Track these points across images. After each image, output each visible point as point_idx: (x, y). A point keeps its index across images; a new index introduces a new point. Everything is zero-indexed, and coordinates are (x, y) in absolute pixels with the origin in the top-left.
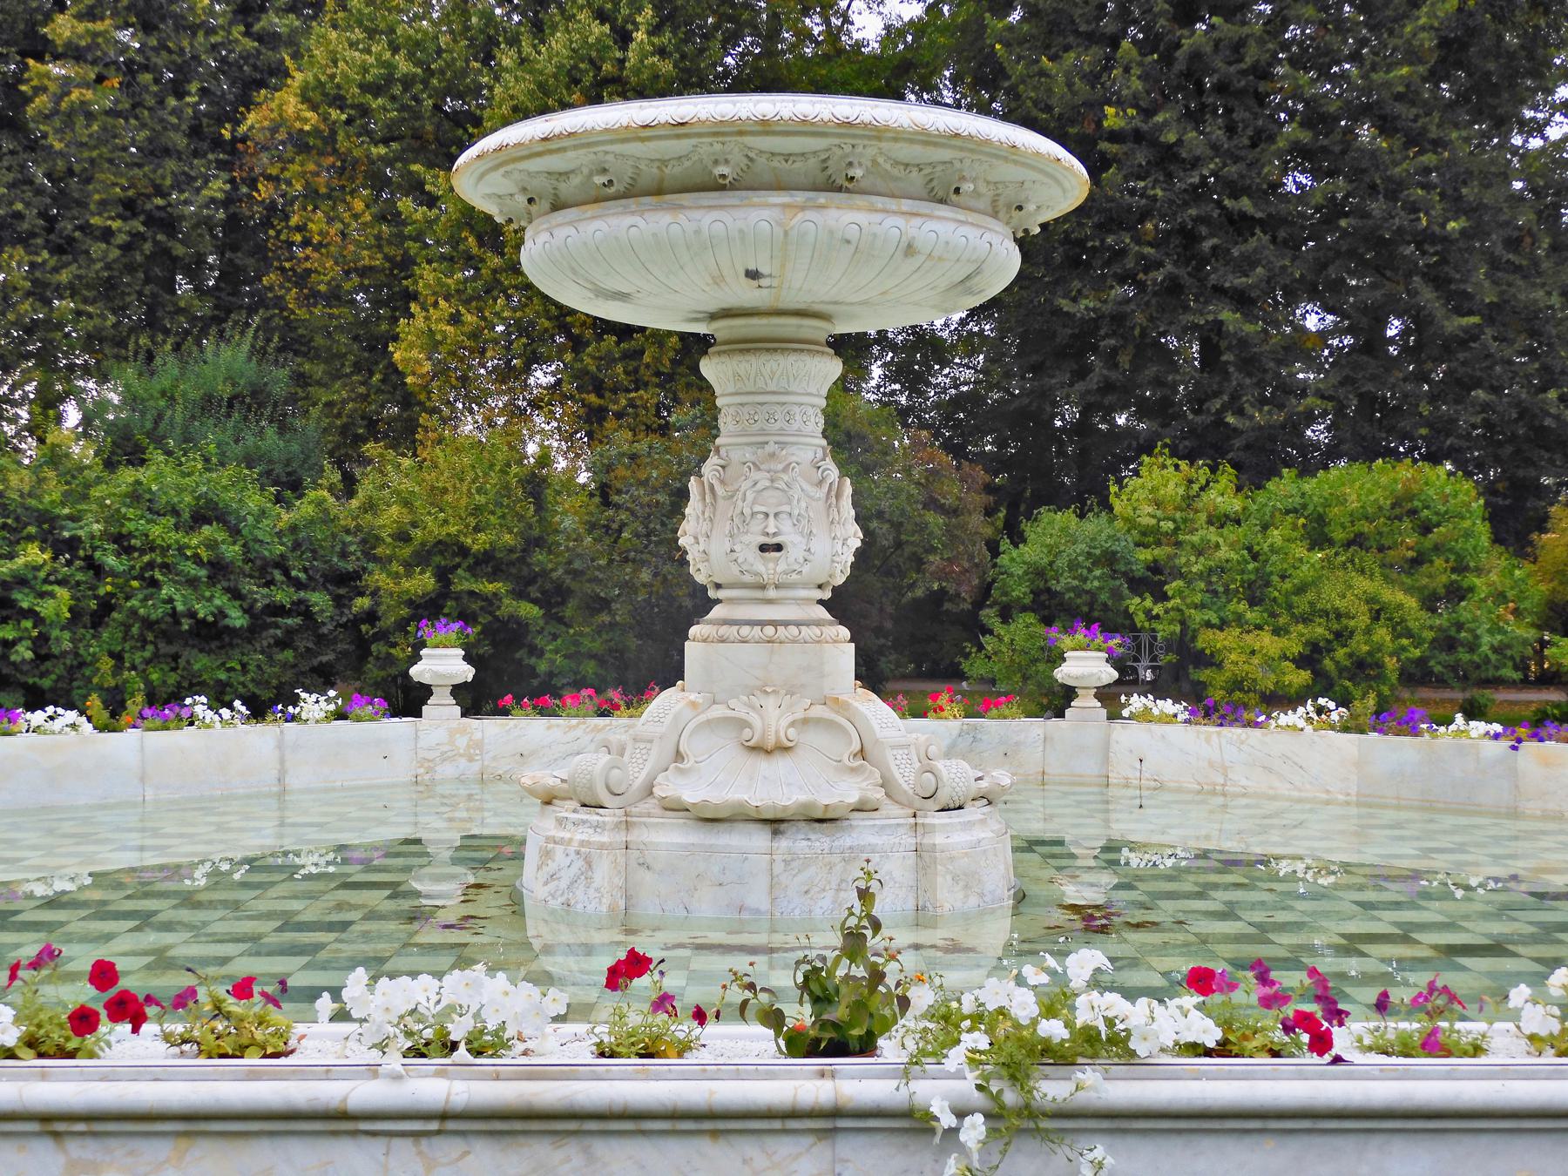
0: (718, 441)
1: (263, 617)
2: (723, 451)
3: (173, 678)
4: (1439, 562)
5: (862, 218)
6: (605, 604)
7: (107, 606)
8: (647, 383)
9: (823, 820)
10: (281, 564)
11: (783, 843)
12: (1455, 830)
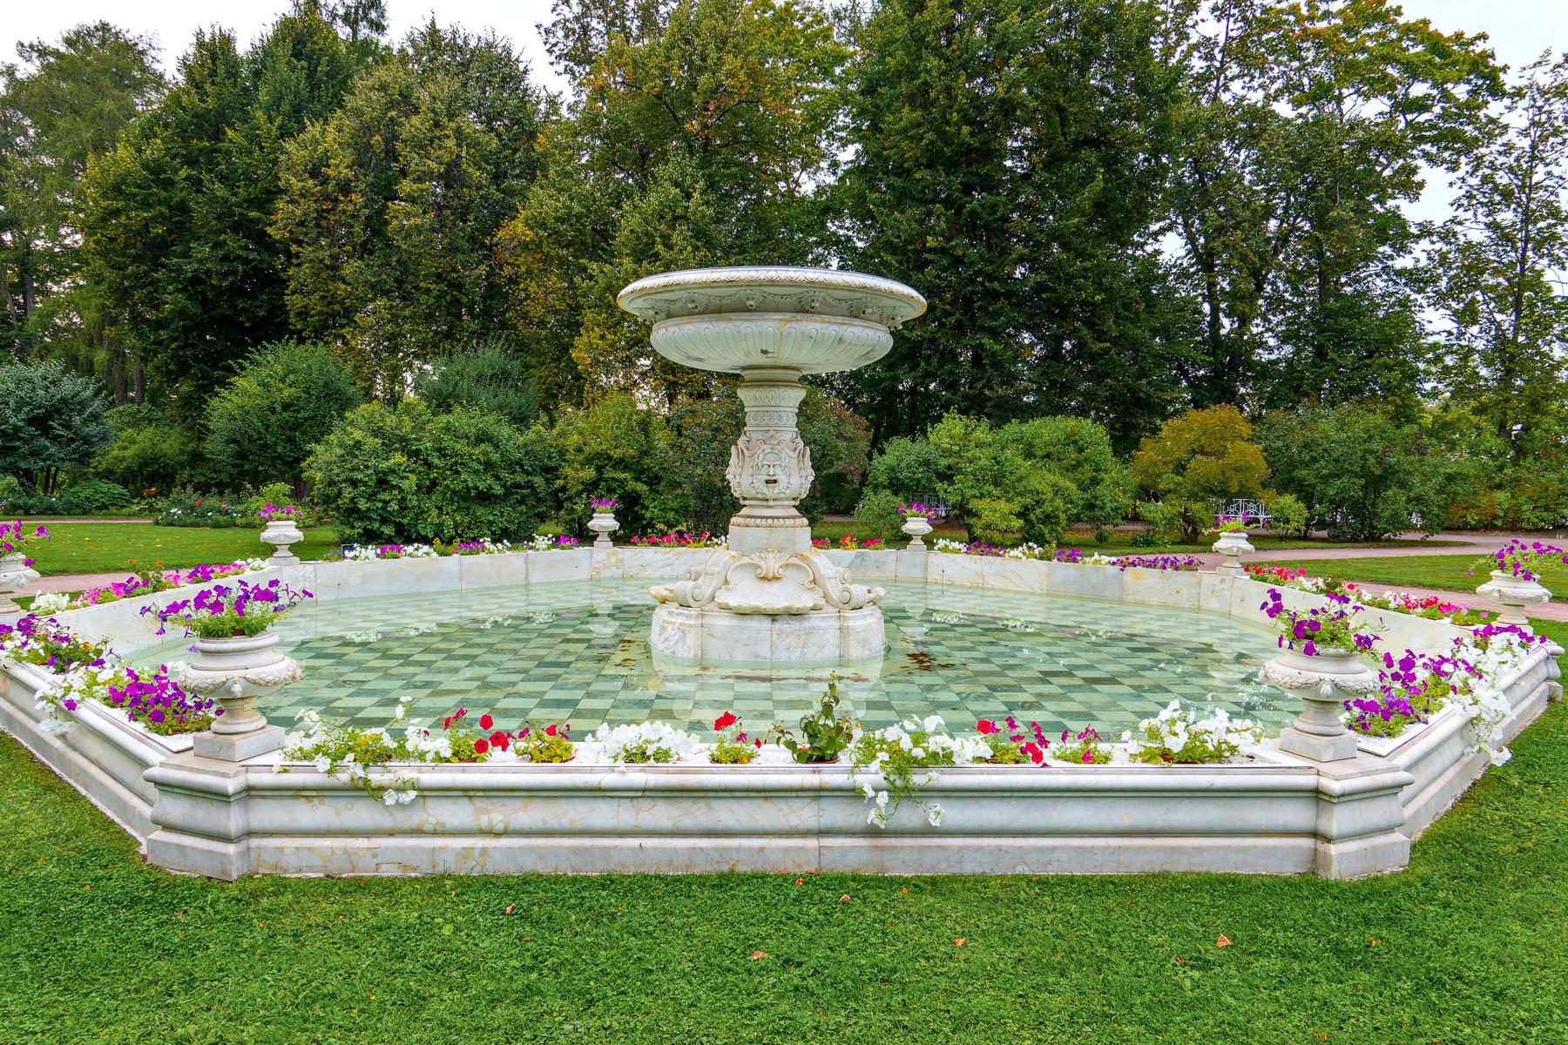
1: (510, 490)
3: (467, 519)
4: (1087, 467)
5: (818, 326)
6: (679, 485)
7: (434, 483)
8: (711, 404)
9: (796, 615)
10: (519, 463)
11: (777, 625)
12: (1096, 610)
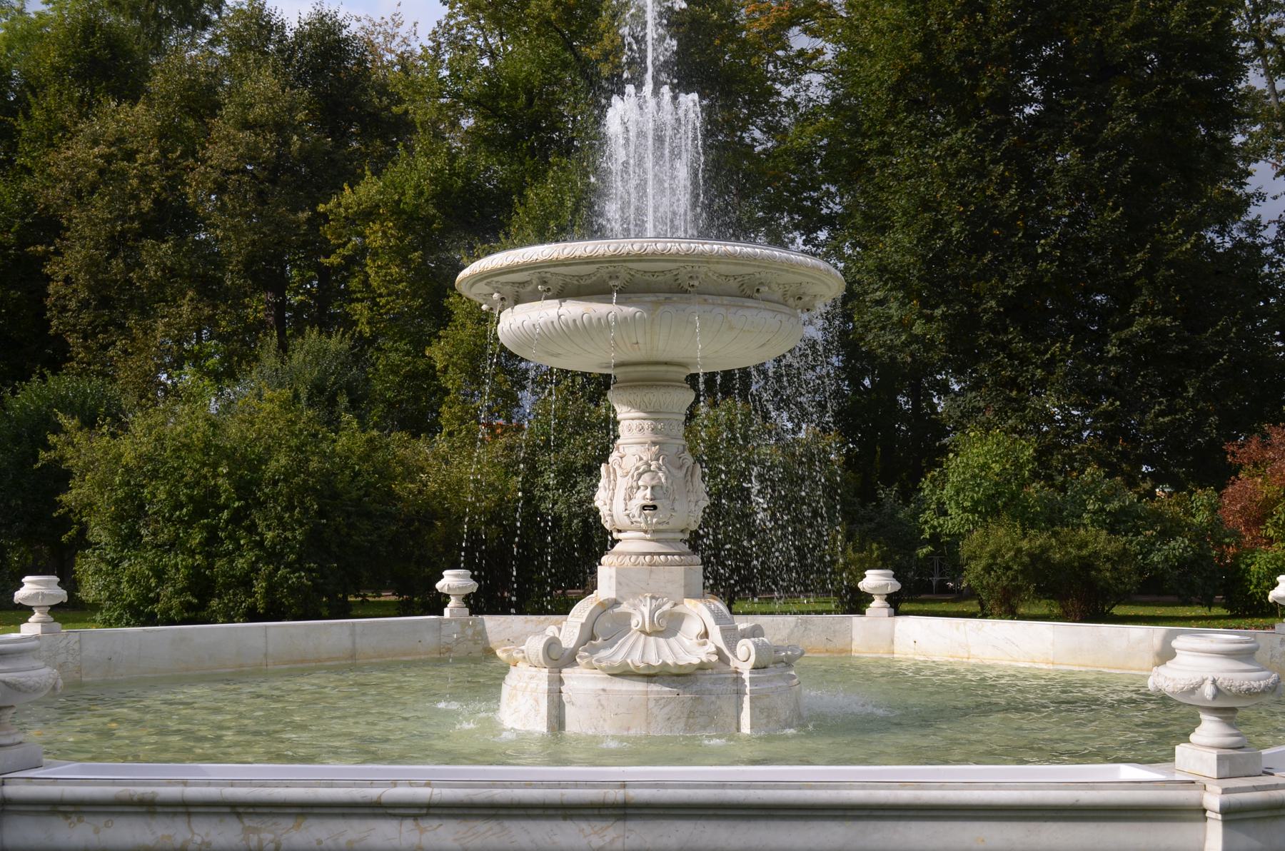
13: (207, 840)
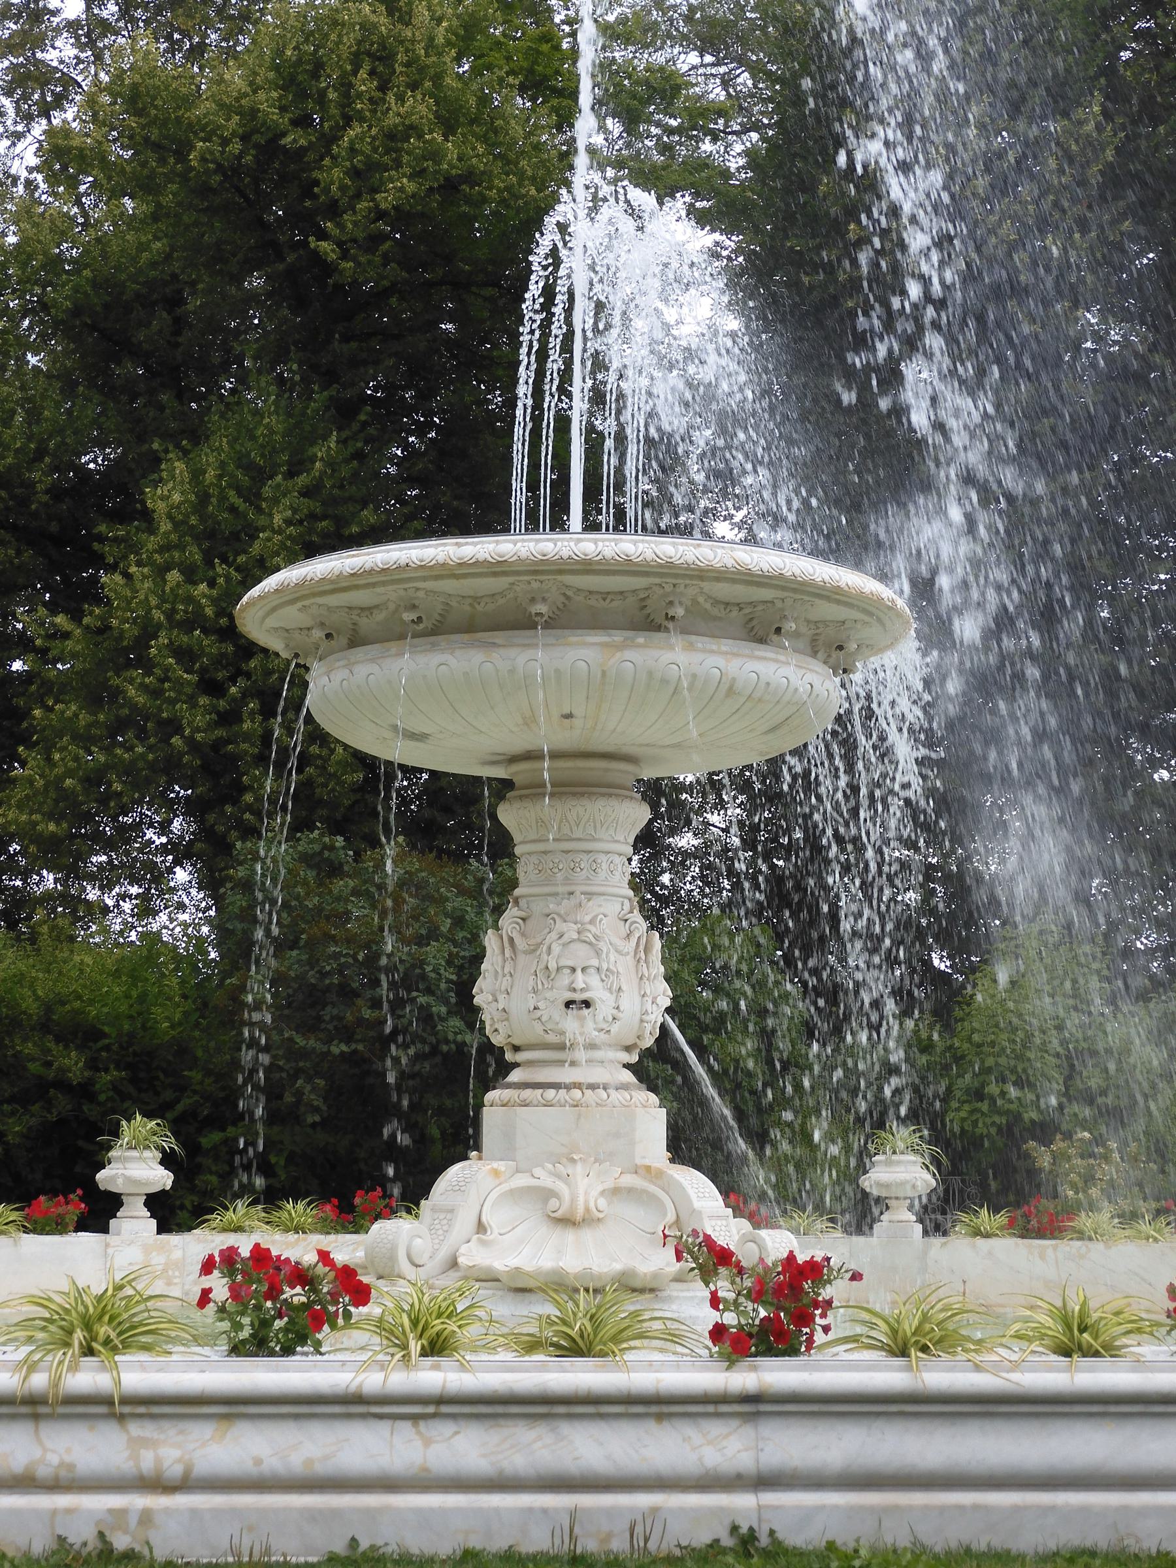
0: (517, 892)
2: (522, 902)
13: (67, 1459)
